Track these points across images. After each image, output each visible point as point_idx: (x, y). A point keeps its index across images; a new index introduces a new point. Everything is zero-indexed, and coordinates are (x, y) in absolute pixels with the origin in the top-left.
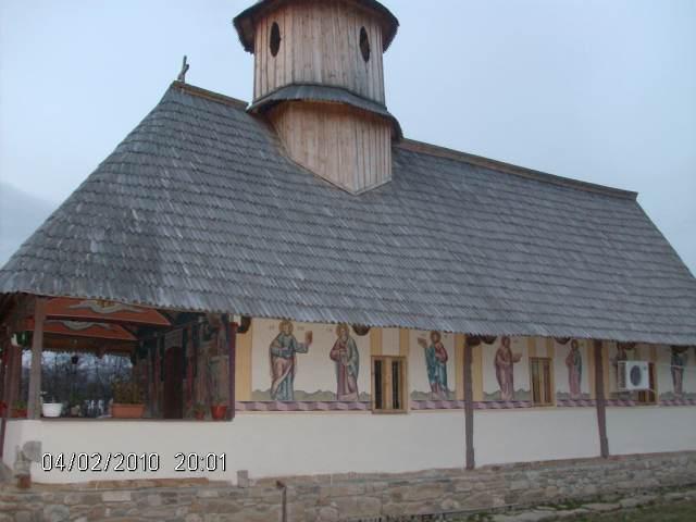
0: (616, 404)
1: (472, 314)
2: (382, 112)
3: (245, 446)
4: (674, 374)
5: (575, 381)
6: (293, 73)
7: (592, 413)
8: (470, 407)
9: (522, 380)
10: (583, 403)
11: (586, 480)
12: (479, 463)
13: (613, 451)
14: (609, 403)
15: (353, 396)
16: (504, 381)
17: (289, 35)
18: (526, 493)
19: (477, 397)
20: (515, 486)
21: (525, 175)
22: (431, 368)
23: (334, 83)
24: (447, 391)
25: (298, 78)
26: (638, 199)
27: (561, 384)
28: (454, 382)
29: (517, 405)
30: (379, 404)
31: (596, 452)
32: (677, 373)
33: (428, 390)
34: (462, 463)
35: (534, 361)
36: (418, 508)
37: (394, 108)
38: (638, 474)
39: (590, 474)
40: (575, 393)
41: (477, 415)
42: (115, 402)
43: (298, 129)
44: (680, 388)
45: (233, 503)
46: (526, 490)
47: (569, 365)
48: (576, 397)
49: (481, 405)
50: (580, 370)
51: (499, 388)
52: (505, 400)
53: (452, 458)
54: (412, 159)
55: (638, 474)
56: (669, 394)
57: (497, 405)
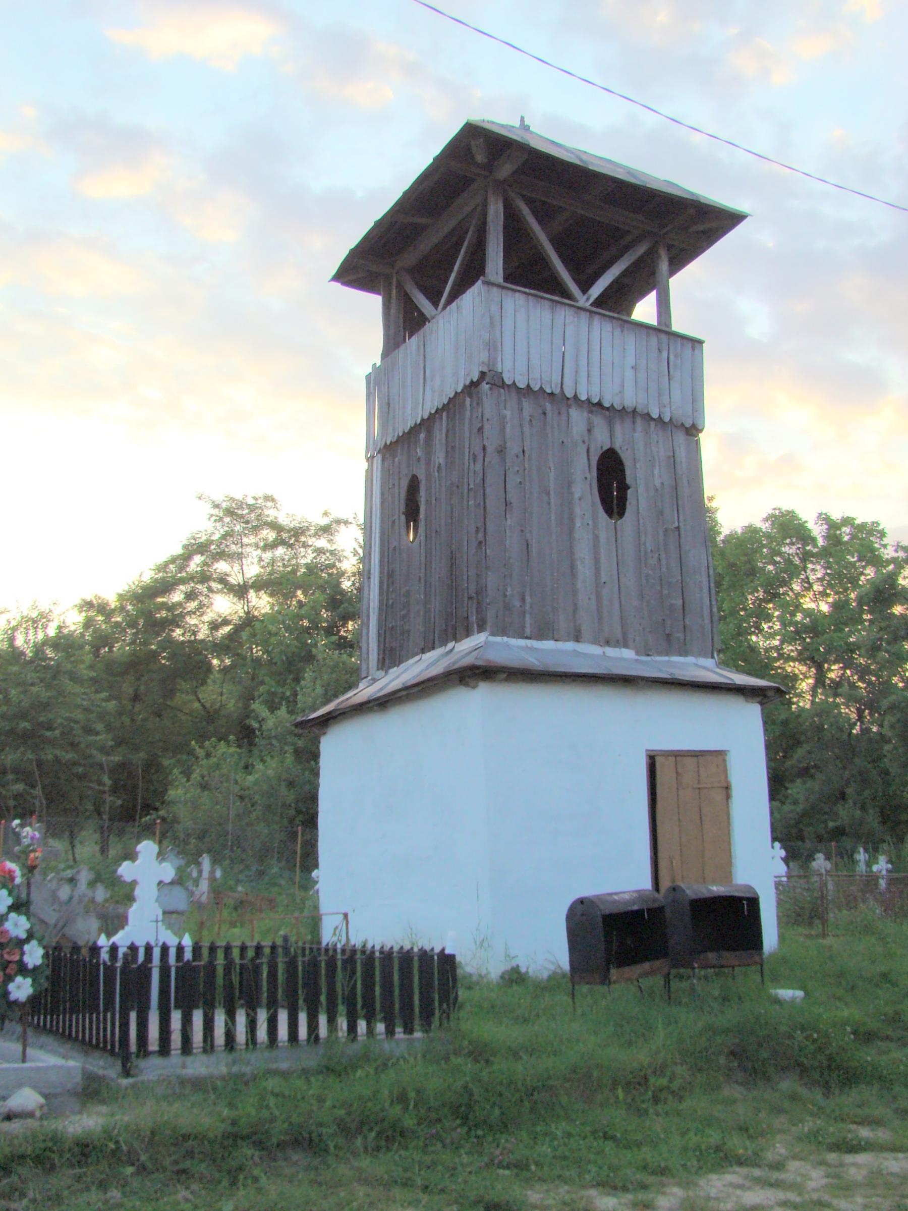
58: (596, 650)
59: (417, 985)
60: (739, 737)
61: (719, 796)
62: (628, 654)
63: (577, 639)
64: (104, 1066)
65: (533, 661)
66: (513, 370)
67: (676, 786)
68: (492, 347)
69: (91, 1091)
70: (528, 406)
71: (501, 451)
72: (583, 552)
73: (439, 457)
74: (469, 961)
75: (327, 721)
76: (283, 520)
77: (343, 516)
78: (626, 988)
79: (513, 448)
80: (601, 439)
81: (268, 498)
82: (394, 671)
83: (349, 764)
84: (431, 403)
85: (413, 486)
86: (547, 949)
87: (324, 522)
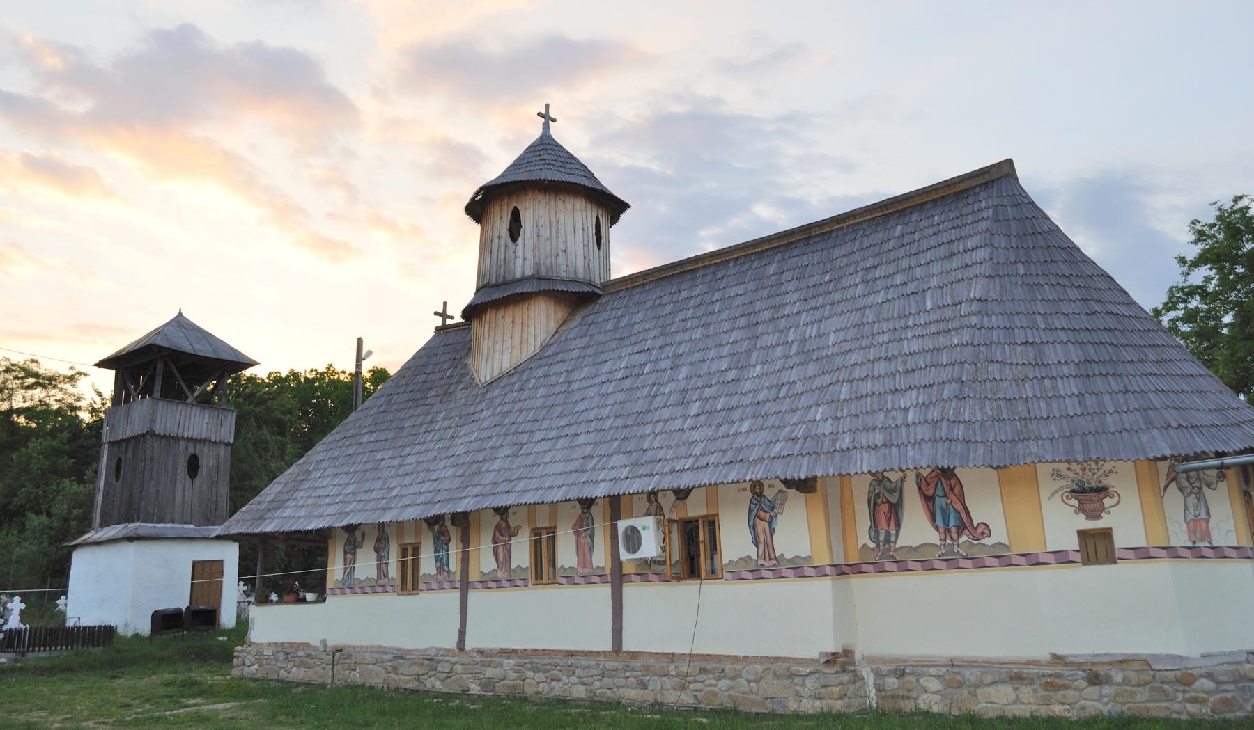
0: (644, 578)
4: (753, 528)
5: (584, 552)
8: (466, 586)
9: (521, 554)
10: (594, 579)
11: (574, 679)
12: (469, 646)
13: (628, 645)
14: (634, 578)
16: (501, 558)
19: (474, 576)
20: (490, 672)
21: (963, 186)
24: (449, 572)
27: (567, 556)
28: (454, 565)
29: (512, 583)
30: (539, 576)
31: (604, 643)
32: (762, 526)
33: (434, 572)
34: (452, 643)
35: (536, 532)
36: (407, 682)
38: (655, 683)
39: (578, 671)
40: (585, 567)
44: (770, 546)
45: (311, 661)
47: (578, 534)
48: (586, 571)
49: (634, 578)
50: (592, 537)
51: (495, 566)
52: (505, 579)
53: (816, 641)
55: (655, 683)
56: (747, 559)
57: (493, 585)
58: (179, 526)
59: (105, 634)
60: (230, 555)
61: (1101, 284)
62: (192, 526)
63: (173, 522)
64: (19, 657)
65: (153, 533)
66: (158, 429)
67: (206, 573)
68: (153, 421)
69: (16, 660)
70: (163, 441)
71: (152, 459)
72: (179, 493)
73: (130, 455)
74: (121, 631)
75: (75, 547)
76: (41, 371)
77: (83, 371)
78: (167, 636)
79: (156, 457)
80: (191, 450)
81: (33, 361)
82: (106, 529)
83: (83, 565)
84: (128, 435)
85: (119, 461)
86: (145, 628)
87: (70, 373)
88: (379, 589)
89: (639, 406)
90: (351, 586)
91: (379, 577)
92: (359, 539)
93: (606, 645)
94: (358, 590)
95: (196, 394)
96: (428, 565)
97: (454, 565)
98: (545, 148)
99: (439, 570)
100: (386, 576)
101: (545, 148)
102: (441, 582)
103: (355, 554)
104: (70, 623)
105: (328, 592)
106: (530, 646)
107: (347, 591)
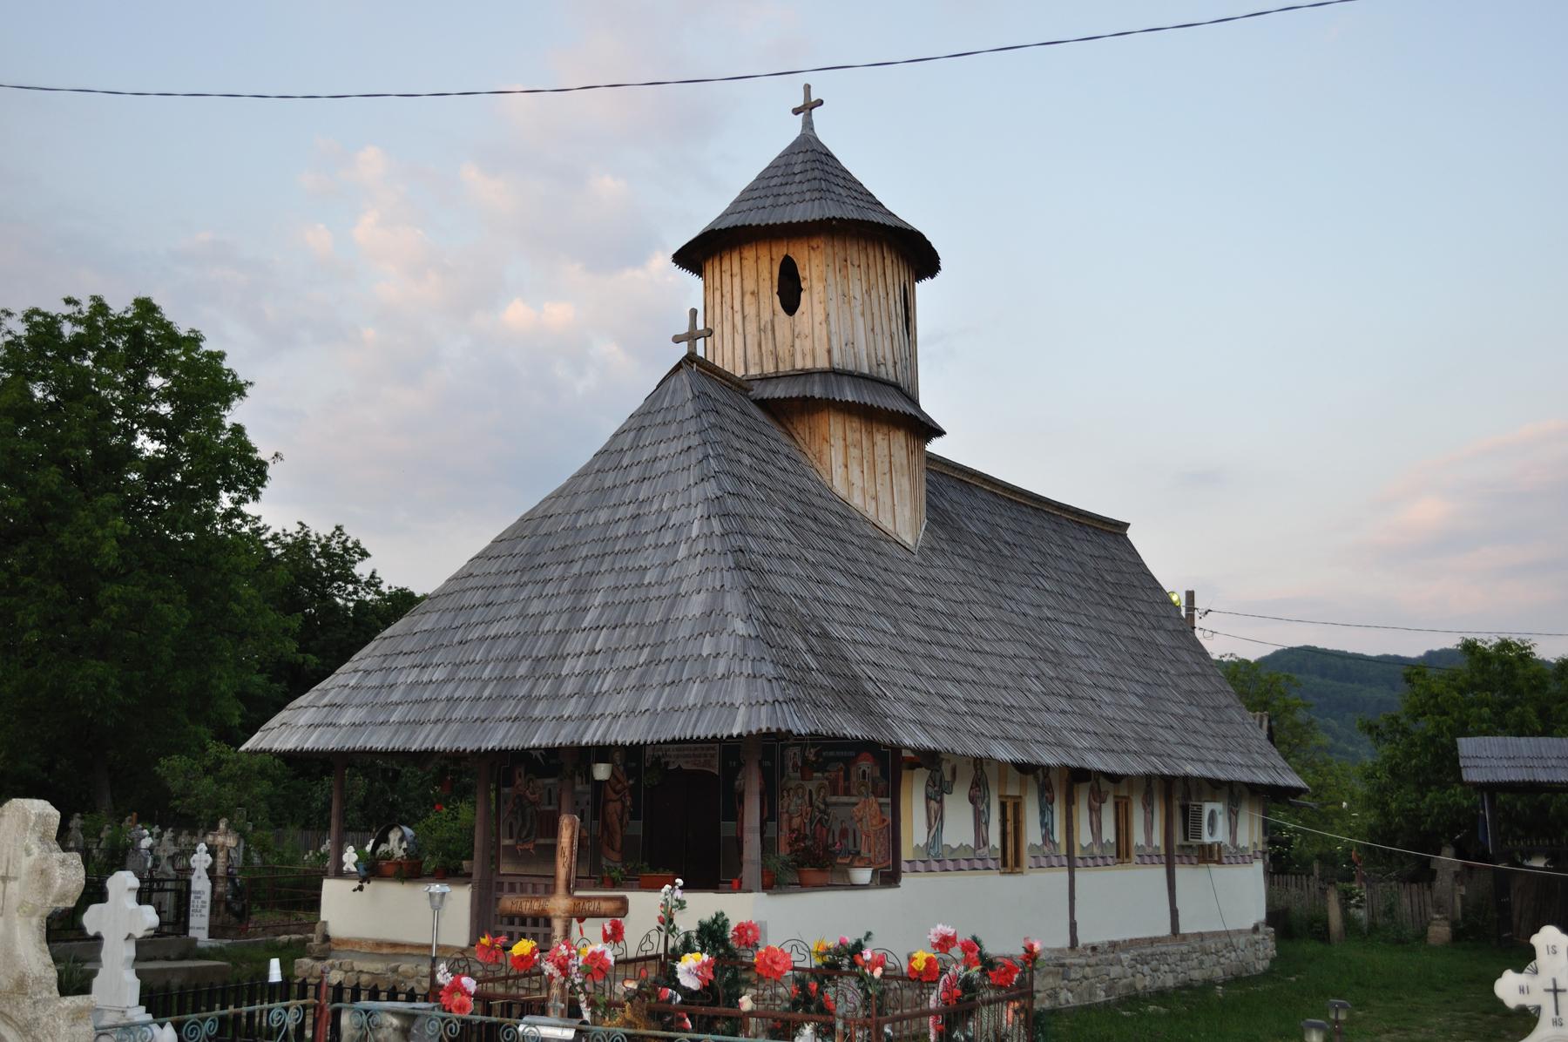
1: (1095, 743)
2: (910, 410)
3: (900, 920)
6: (829, 352)
7: (1160, 872)
13: (1183, 930)
15: (985, 850)
17: (818, 287)
18: (199, 924)
22: (1042, 813)
23: (883, 375)
25: (838, 361)
26: (1131, 534)
33: (1039, 842)
37: (931, 404)
41: (1078, 874)
42: (228, 826)
43: (838, 443)
46: (176, 919)
47: (972, 800)
54: (957, 492)
88: (978, 864)
89: (543, 647)
90: (938, 859)
91: (977, 846)
92: (948, 777)
93: (1165, 930)
94: (950, 865)
95: (225, 1012)
96: (1032, 833)
97: (1059, 836)
98: (810, 162)
99: (1044, 838)
100: (986, 843)
101: (810, 162)
102: (1045, 861)
103: (941, 802)
104: (275, 513)
105: (904, 866)
106: (1128, 936)
107: (935, 865)
